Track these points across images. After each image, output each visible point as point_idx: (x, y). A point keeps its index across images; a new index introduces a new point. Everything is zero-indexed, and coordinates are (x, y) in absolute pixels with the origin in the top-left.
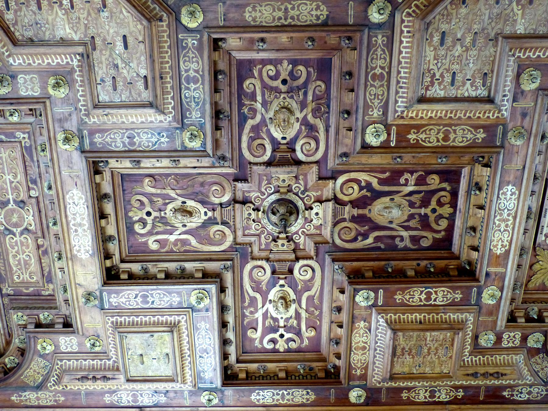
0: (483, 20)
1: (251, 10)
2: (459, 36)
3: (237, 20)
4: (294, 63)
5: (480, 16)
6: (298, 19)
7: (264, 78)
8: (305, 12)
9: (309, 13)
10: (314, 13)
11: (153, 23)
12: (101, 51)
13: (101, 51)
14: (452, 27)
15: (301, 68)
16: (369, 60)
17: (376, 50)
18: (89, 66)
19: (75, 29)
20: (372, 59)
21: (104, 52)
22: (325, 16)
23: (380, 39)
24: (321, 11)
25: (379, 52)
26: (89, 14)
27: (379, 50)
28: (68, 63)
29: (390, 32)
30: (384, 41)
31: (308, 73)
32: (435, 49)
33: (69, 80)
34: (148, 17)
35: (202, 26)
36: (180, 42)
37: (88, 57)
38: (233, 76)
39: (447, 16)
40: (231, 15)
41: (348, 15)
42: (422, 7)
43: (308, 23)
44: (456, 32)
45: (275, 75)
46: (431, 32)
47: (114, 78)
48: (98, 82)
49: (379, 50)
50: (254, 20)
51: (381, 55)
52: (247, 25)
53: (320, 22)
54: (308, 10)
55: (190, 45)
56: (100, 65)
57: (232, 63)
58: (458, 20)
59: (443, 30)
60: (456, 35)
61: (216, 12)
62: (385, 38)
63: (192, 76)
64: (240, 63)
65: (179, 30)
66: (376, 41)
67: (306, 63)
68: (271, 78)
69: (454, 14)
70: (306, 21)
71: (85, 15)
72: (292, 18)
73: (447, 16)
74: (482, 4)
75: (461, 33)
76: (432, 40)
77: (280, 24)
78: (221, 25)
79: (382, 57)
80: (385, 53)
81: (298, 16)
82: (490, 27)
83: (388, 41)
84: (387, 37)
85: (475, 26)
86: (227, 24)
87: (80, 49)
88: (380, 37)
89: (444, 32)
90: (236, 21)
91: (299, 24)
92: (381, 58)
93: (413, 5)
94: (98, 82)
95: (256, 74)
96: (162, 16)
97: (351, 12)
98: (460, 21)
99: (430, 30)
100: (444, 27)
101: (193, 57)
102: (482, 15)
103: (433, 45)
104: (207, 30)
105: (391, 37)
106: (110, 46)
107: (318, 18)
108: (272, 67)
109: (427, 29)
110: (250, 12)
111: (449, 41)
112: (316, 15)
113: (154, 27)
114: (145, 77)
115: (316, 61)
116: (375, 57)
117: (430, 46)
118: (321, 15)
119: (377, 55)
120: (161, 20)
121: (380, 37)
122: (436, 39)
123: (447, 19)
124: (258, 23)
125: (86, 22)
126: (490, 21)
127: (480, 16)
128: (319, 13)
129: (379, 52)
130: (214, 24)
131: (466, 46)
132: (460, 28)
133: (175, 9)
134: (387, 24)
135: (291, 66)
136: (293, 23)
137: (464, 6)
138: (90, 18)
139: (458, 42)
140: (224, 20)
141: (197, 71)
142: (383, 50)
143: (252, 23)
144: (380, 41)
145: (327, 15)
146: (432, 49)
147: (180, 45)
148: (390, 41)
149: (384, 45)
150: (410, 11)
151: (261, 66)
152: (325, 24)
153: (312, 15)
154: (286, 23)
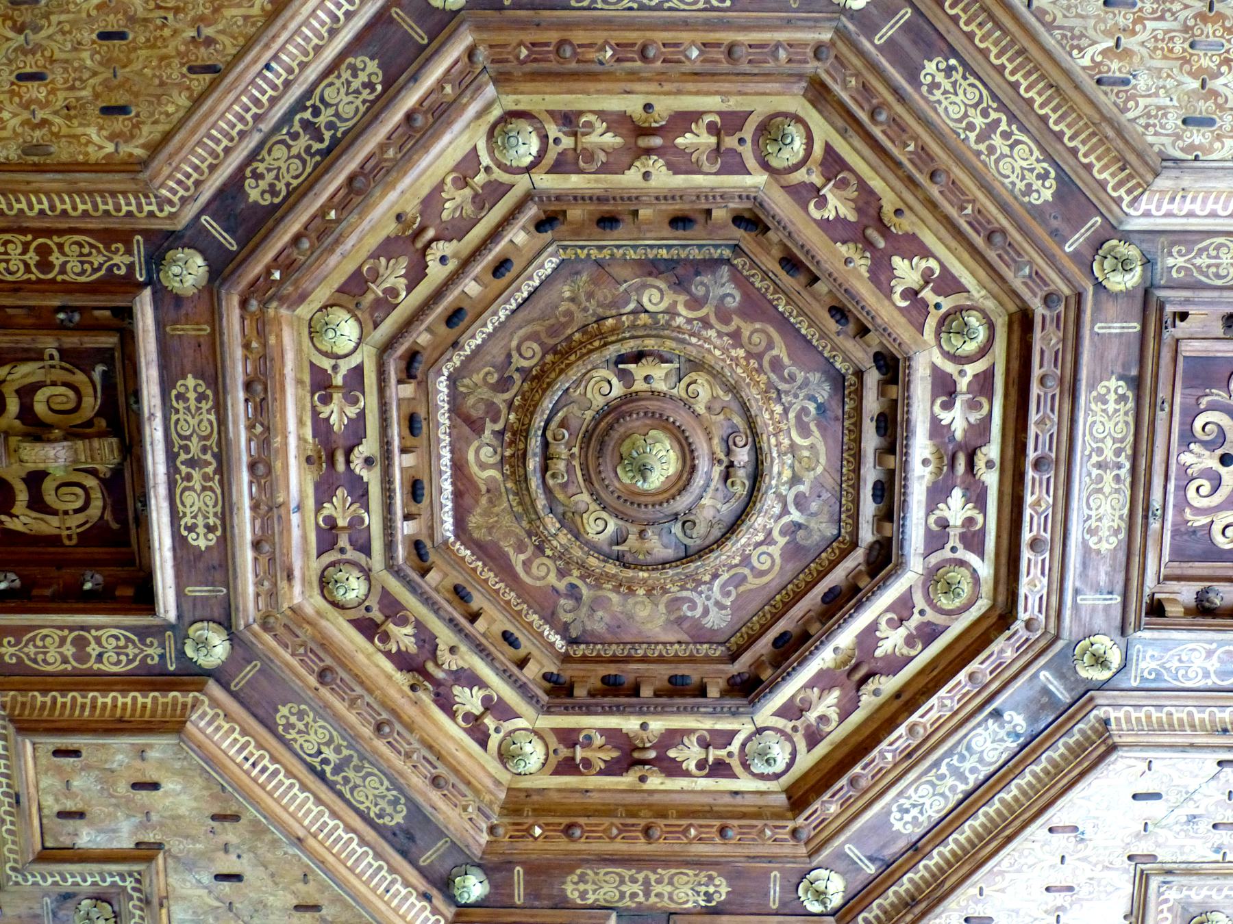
0: (1166, 32)
1: (1095, 539)
2: (1196, 84)
3: (1113, 567)
4: (1188, 437)
5: (1156, 40)
6: (1122, 441)
7: (1214, 504)
8: (1110, 425)
9: (1110, 418)
10: (1111, 406)
11: (1117, 739)
12: (1158, 845)
13: (1158, 845)
14: (1175, 103)
15: (1198, 424)
16: (1219, 283)
17: (1199, 268)
18: (1188, 873)
19: (1110, 889)
20: (1218, 276)
21: (1160, 840)
22: (1121, 383)
23: (1175, 261)
24: (1109, 391)
25: (1203, 261)
26: (1084, 859)
27: (1198, 261)
28: (1170, 910)
29: (1163, 239)
30: (1179, 252)
31: (1212, 407)
32: (1219, 138)
33: (1198, 911)
34: (1103, 748)
35: (1118, 639)
36: (1148, 685)
37: (1169, 872)
38: (1205, 572)
39: (1149, 116)
40: (1103, 579)
41: (1121, 334)
42: (1123, 174)
43: (1131, 419)
44: (1187, 93)
45: (1209, 479)
46: (1182, 150)
47: (1215, 826)
48: (1219, 857)
49: (1198, 261)
50: (1117, 532)
51: (1209, 257)
52: (1124, 546)
53: (1130, 394)
54: (1105, 420)
55: (1154, 665)
56: (1186, 850)
57: (1178, 572)
58: (1162, 91)
59: (1179, 122)
60: (1194, 91)
61: (1094, 609)
62: (1175, 250)
63: (1217, 665)
64: (1179, 554)
65: (1123, 686)
66: (1178, 271)
67: (1191, 414)
68: (1215, 489)
69: (1148, 101)
70: (1127, 423)
71: (1088, 867)
72: (1118, 453)
73: (1149, 116)
74: (1133, 39)
75: (1188, 79)
76: (1200, 147)
77: (1129, 480)
78: (1119, 599)
79: (1214, 253)
80: (1206, 249)
81: (1115, 441)
82: (1182, 16)
83: (1179, 243)
84: (1173, 244)
85: (1178, 49)
86: (1119, 587)
87: (1154, 883)
88: (1170, 262)
89: (1185, 122)
90: (1114, 570)
91: (1131, 438)
92: (1217, 257)
93: (1115, 194)
94: (1219, 857)
95: (1203, 520)
96: (1099, 720)
97: (1116, 328)
98: (1164, 87)
99: (1178, 154)
100: (1173, 121)
101: (1180, 660)
102: (1155, 37)
103: (1211, 144)
104: (1130, 630)
105: (1172, 238)
106: (1150, 828)
107: (1122, 398)
108: (1192, 487)
109: (1175, 160)
110: (1100, 541)
111: (1204, 107)
112: (1117, 402)
113: (1124, 739)
114: (1220, 763)
115: (1188, 391)
116: (1213, 269)
117: (1211, 150)
118: (369, 75)
119: (1208, 266)
120: (1106, 722)
121: (1170, 262)
122: (1197, 136)
123: (1156, 117)
124: (1123, 525)
125: (1100, 867)
126: (1168, 15)
127: (1156, 40)
128: (1112, 397)
129: (1203, 261)
130: (1117, 613)
131: (1219, 66)
132: (1180, 84)
133: (1081, 690)
134: (1144, 246)
135: (1192, 446)
136: (1129, 452)
137: (1133, 82)
138: (1093, 859)
139: (1211, 84)
140: (1110, 593)
141: (1210, 654)
142: (1201, 251)
143: (1122, 536)
144: (1180, 261)
145: (1120, 378)
146: (1217, 145)
147: (1153, 685)
148: (1182, 237)
149: (1189, 252)
150: (1127, 199)
151: (1188, 510)
152: (1137, 384)
153: (1116, 411)
154: (1128, 465)
